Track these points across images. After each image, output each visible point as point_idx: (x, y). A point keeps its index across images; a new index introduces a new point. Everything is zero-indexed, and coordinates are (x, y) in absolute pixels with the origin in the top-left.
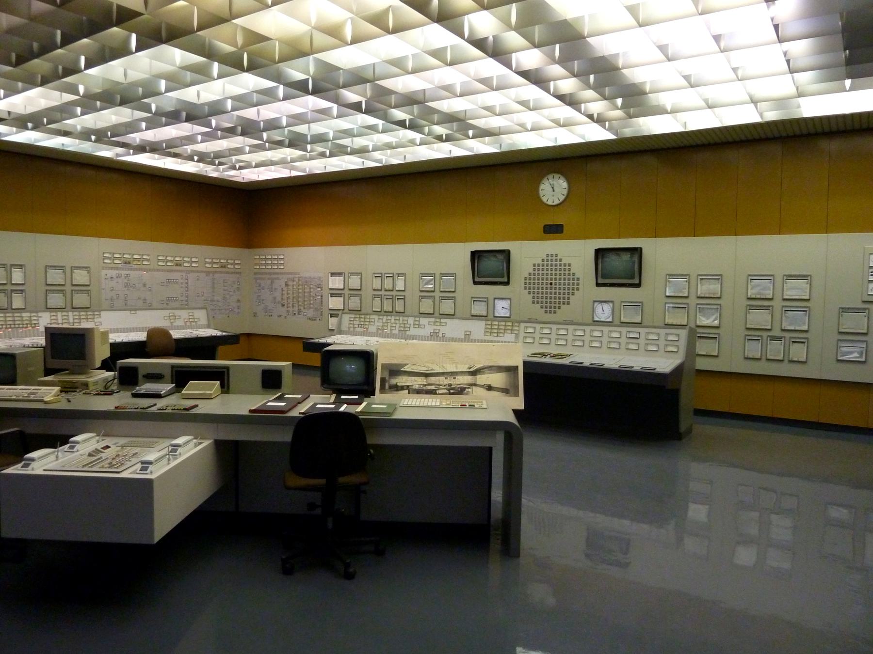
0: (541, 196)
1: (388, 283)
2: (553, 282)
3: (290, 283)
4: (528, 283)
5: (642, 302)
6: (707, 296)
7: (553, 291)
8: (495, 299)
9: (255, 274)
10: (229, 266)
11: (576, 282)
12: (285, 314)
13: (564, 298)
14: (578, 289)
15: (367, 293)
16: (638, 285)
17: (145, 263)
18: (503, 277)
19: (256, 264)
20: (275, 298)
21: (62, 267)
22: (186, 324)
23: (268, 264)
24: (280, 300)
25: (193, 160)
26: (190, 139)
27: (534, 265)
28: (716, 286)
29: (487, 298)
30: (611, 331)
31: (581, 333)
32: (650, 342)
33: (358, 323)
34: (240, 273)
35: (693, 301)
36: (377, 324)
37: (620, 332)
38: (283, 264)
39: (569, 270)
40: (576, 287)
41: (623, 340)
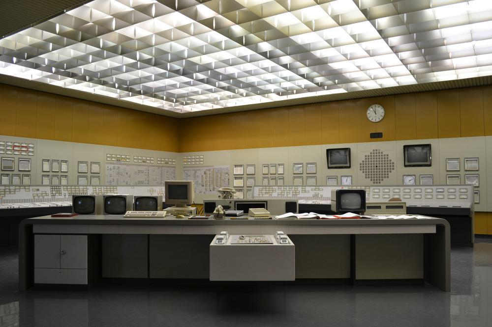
0: (368, 117)
1: (273, 170)
2: (378, 165)
3: (208, 172)
4: (363, 167)
5: (432, 175)
6: (471, 169)
7: (378, 170)
8: (342, 176)
9: (184, 167)
10: (170, 163)
11: (392, 165)
12: (204, 191)
13: (385, 174)
14: (393, 169)
15: (259, 177)
16: (349, 167)
17: (127, 160)
18: (347, 163)
19: (185, 162)
20: (197, 181)
21: (86, 162)
22: (34, 198)
23: (197, 161)
24: (201, 182)
25: (85, 80)
26: (84, 60)
27: (366, 156)
28: (476, 164)
29: (337, 176)
30: (449, 189)
31: (408, 191)
32: (416, 193)
33: (265, 191)
34: (175, 167)
35: (462, 173)
36: (277, 191)
37: (432, 189)
38: (203, 158)
39: (388, 158)
40: (392, 167)
41: (435, 193)
